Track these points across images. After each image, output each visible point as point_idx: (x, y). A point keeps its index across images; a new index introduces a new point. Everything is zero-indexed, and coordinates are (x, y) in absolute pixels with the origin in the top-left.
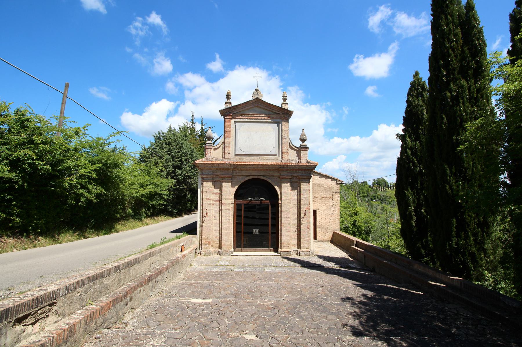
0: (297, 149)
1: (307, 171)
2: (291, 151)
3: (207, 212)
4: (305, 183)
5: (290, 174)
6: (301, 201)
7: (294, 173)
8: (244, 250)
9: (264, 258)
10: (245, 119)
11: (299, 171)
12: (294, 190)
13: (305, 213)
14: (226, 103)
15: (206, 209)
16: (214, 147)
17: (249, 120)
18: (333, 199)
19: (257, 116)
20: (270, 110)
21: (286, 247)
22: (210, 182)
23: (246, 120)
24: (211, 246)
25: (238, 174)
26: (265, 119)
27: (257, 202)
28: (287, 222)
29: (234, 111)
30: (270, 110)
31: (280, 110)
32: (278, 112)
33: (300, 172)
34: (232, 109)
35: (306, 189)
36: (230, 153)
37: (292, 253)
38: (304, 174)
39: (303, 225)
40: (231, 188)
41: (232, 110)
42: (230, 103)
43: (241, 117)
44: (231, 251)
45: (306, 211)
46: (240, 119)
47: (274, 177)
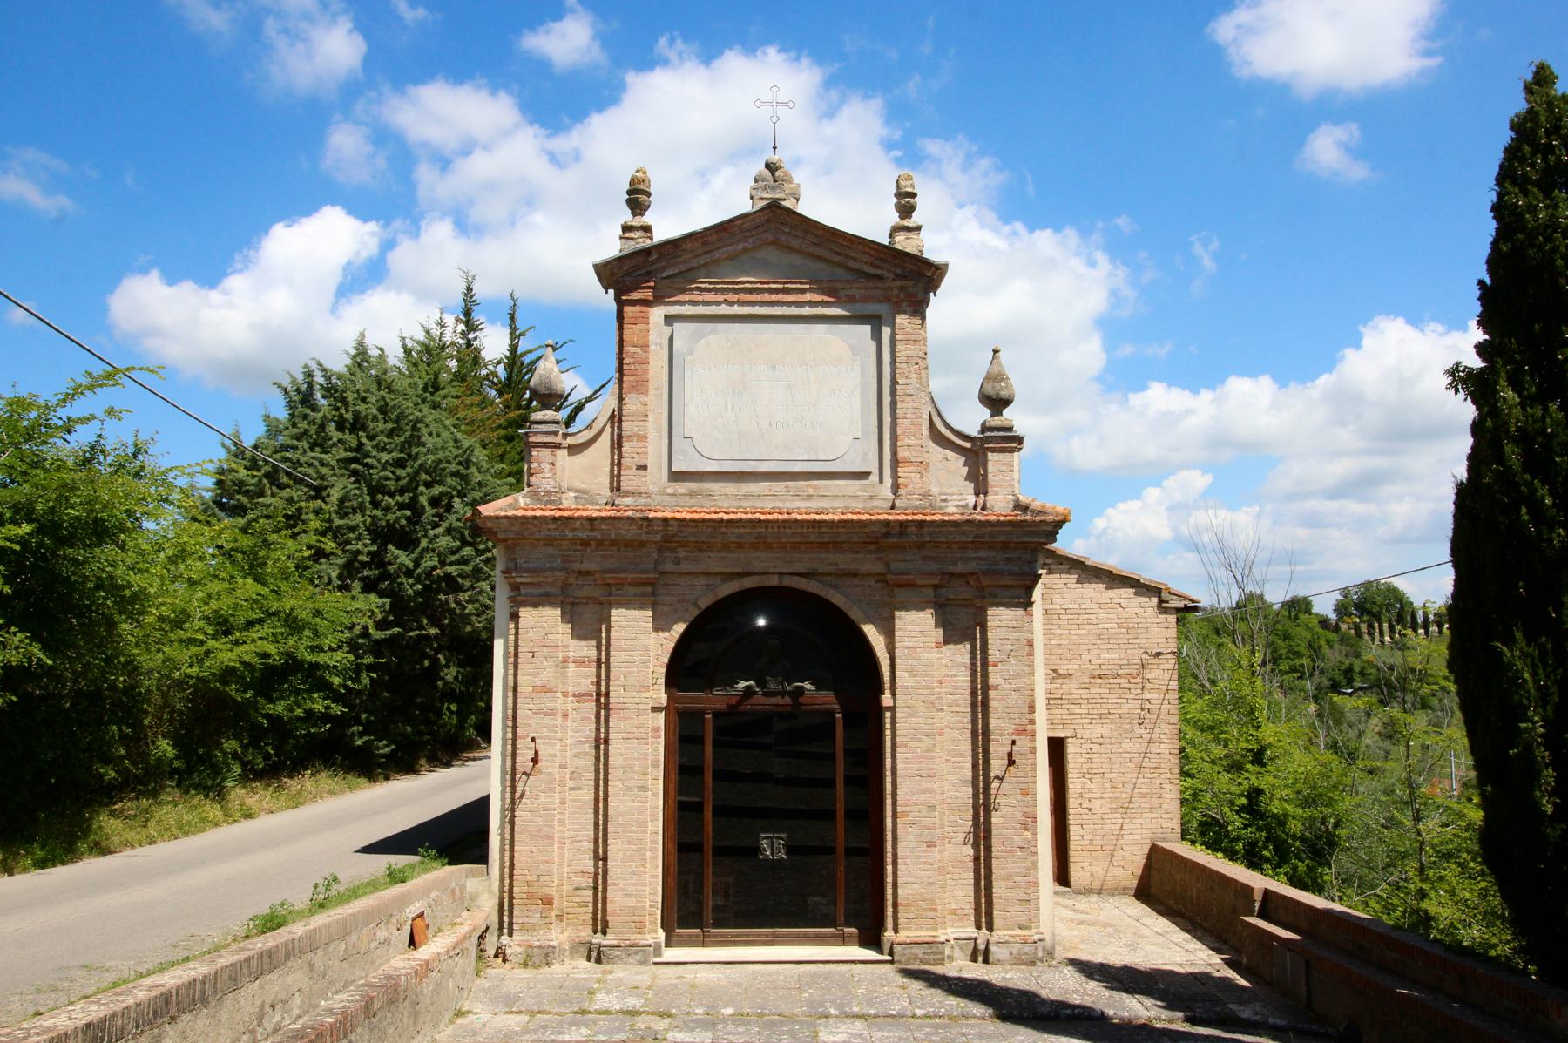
0: (968, 445)
2: (937, 452)
3: (536, 753)
4: (1008, 606)
5: (935, 566)
6: (992, 693)
7: (954, 562)
9: (814, 975)
10: (718, 303)
12: (956, 642)
13: (1010, 754)
14: (626, 228)
15: (533, 739)
16: (570, 440)
17: (737, 310)
18: (1148, 686)
19: (777, 291)
23: (724, 309)
26: (811, 304)
27: (778, 700)
28: (923, 797)
29: (664, 268)
33: (982, 554)
34: (654, 257)
35: (1012, 635)
36: (644, 468)
37: (947, 952)
39: (1004, 810)
40: (653, 635)
41: (653, 263)
42: (647, 229)
43: (695, 296)
44: (651, 941)
45: (1014, 742)
46: (693, 303)
47: (856, 581)
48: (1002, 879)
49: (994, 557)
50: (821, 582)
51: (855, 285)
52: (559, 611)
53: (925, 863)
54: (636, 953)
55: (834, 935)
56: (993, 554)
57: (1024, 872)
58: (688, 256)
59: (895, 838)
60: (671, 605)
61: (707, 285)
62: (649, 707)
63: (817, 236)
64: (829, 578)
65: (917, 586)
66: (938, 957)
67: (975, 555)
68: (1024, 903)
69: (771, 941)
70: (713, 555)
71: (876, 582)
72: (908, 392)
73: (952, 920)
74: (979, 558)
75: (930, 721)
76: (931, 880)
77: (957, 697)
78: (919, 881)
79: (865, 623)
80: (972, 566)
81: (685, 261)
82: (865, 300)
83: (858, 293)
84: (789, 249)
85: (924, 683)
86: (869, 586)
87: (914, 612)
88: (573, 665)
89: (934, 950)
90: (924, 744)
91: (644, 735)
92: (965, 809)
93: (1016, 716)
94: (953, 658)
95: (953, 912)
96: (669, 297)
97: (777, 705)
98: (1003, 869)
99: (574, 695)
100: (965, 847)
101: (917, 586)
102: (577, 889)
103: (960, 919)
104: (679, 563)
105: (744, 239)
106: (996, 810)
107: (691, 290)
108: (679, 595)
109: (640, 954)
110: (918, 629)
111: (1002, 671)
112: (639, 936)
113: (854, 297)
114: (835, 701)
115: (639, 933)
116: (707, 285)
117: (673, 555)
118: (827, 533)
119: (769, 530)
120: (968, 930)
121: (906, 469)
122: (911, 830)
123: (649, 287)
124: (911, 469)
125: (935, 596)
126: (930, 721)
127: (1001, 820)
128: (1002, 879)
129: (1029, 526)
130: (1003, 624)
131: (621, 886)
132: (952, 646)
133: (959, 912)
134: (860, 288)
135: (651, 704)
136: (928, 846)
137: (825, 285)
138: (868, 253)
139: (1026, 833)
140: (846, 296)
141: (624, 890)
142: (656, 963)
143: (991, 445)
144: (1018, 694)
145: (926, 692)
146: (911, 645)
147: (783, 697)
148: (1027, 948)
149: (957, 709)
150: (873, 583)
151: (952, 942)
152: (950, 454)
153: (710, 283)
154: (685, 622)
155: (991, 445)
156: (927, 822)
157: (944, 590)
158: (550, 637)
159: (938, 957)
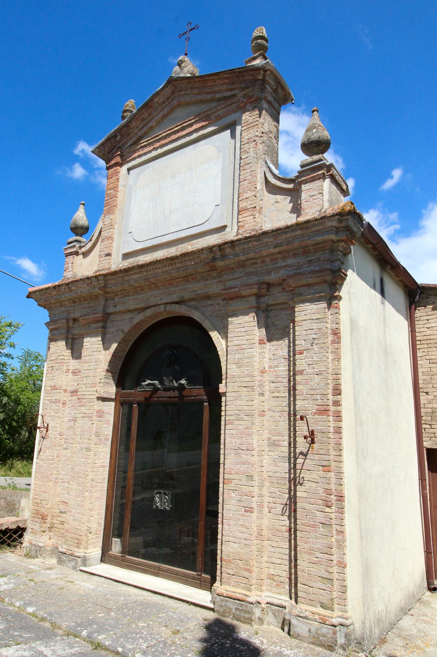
0: (291, 186)
1: (315, 251)
2: (271, 198)
4: (311, 301)
5: (254, 279)
6: (298, 378)
7: (268, 273)
8: (131, 562)
9: (146, 605)
10: (150, 152)
11: (284, 258)
12: (278, 339)
16: (83, 250)
17: (160, 151)
19: (178, 131)
20: (209, 96)
21: (238, 579)
22: (62, 339)
23: (154, 153)
24: (47, 529)
25: (120, 308)
26: (196, 131)
27: (170, 394)
28: (243, 468)
29: (126, 143)
30: (209, 96)
31: (233, 83)
32: (229, 94)
33: (290, 261)
34: (119, 138)
35: (315, 326)
36: (109, 255)
37: (257, 612)
38: (305, 269)
39: (307, 485)
40: (104, 352)
41: (120, 142)
43: (141, 152)
44: (81, 554)
46: (140, 156)
47: (210, 302)
48: (306, 552)
49: (298, 263)
50: (189, 307)
51: (219, 107)
52: (64, 343)
53: (242, 525)
54: (72, 560)
55: (194, 578)
56: (298, 260)
57: (326, 550)
58: (136, 131)
59: (423, 533)
60: (113, 333)
61: (145, 143)
62: (95, 397)
63: (197, 88)
64: (194, 303)
65: (244, 297)
66: (247, 616)
67: (284, 264)
68: (325, 581)
69: (157, 573)
70: (130, 298)
71: (223, 300)
72: (248, 162)
73: (271, 585)
74: (287, 266)
75: (250, 403)
76: (247, 542)
77: (277, 385)
78: (237, 541)
79: (211, 331)
80: (282, 274)
81: (135, 134)
82: (226, 115)
83: (220, 113)
84: (188, 104)
85: (246, 372)
86: (218, 304)
87: (241, 317)
88: (71, 374)
89: (244, 608)
90: (245, 423)
91: (91, 415)
92: (283, 482)
93: (319, 397)
94: (275, 352)
95: (271, 577)
96: (129, 158)
97: (170, 397)
98: (306, 543)
99: (70, 392)
100: (282, 518)
101: (244, 297)
102: (61, 512)
103: (277, 586)
104: (116, 306)
105: (163, 109)
106: (301, 484)
107: (138, 149)
108: (117, 326)
109: (74, 562)
110: (243, 330)
111: (307, 357)
112: (77, 549)
113: (219, 115)
114: (204, 393)
115: (78, 547)
116: (145, 143)
117: (113, 302)
118: (181, 267)
119: (149, 273)
120: (281, 597)
121: (244, 215)
122: (233, 495)
123: (118, 155)
124: (248, 213)
125: (257, 303)
126: (250, 403)
127: (305, 495)
128: (306, 552)
129: (315, 226)
130: (308, 317)
131: (73, 513)
132: (275, 343)
133: (276, 578)
134: (223, 109)
135: (97, 395)
136: (246, 511)
137: (203, 115)
138: (225, 83)
139: (328, 510)
140: (215, 117)
141: (74, 516)
142: (81, 571)
143: (304, 178)
144: (320, 377)
145: (247, 379)
146: (238, 343)
147: (174, 392)
148: (325, 630)
149: (278, 395)
150: (220, 301)
151: (263, 605)
152: (279, 197)
153: (146, 141)
154: (117, 343)
155: (304, 178)
156: (246, 489)
157: (267, 298)
158: (60, 358)
159: (247, 616)
